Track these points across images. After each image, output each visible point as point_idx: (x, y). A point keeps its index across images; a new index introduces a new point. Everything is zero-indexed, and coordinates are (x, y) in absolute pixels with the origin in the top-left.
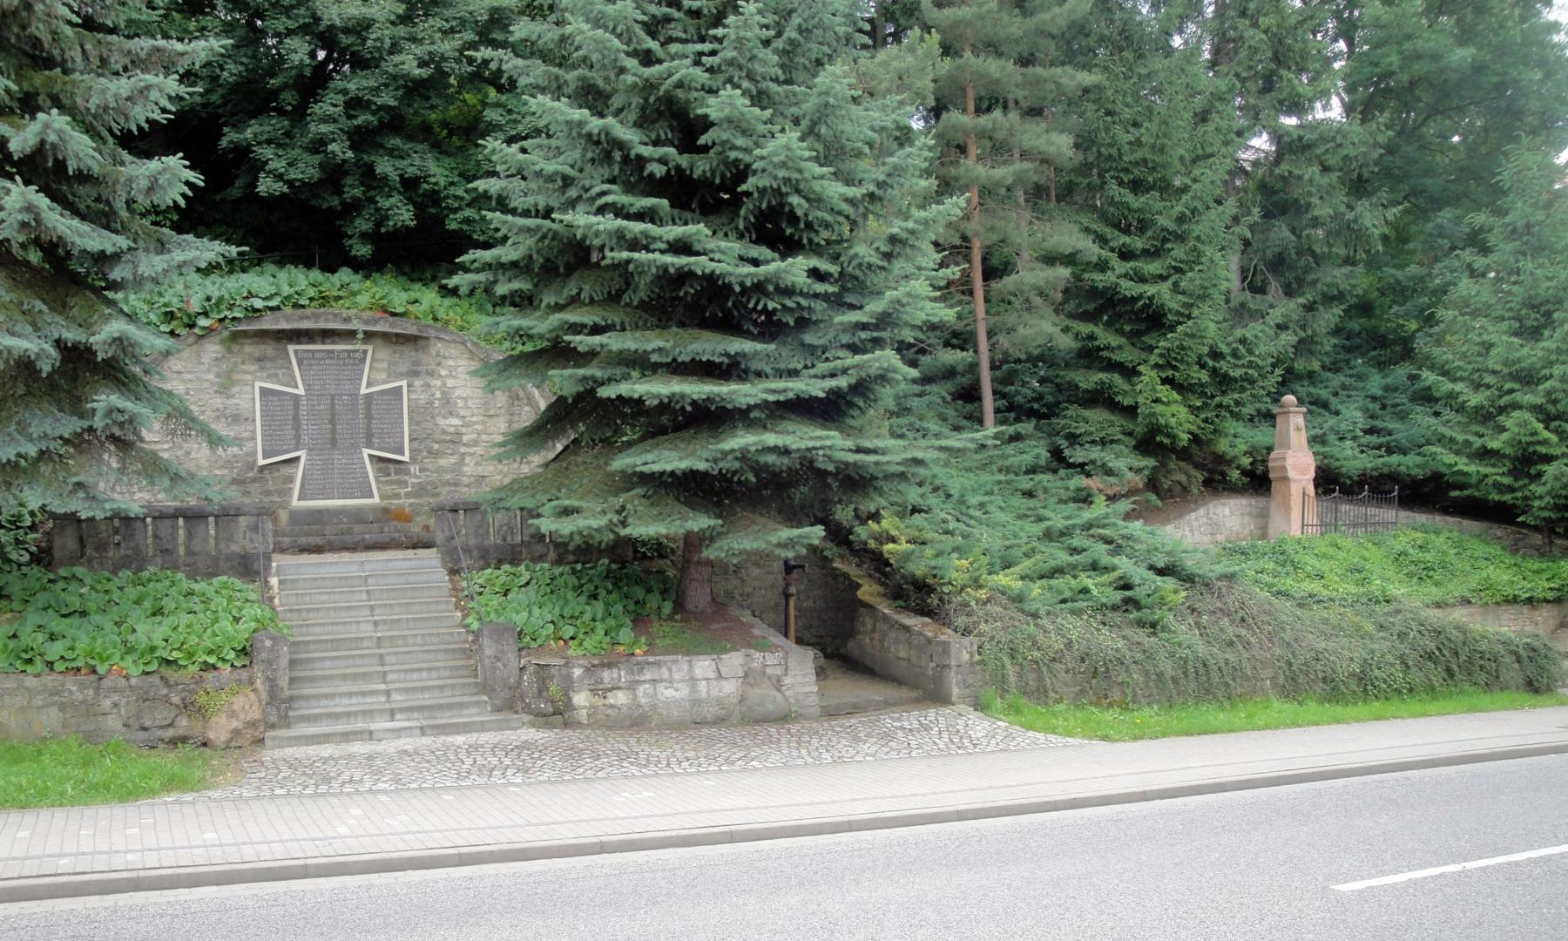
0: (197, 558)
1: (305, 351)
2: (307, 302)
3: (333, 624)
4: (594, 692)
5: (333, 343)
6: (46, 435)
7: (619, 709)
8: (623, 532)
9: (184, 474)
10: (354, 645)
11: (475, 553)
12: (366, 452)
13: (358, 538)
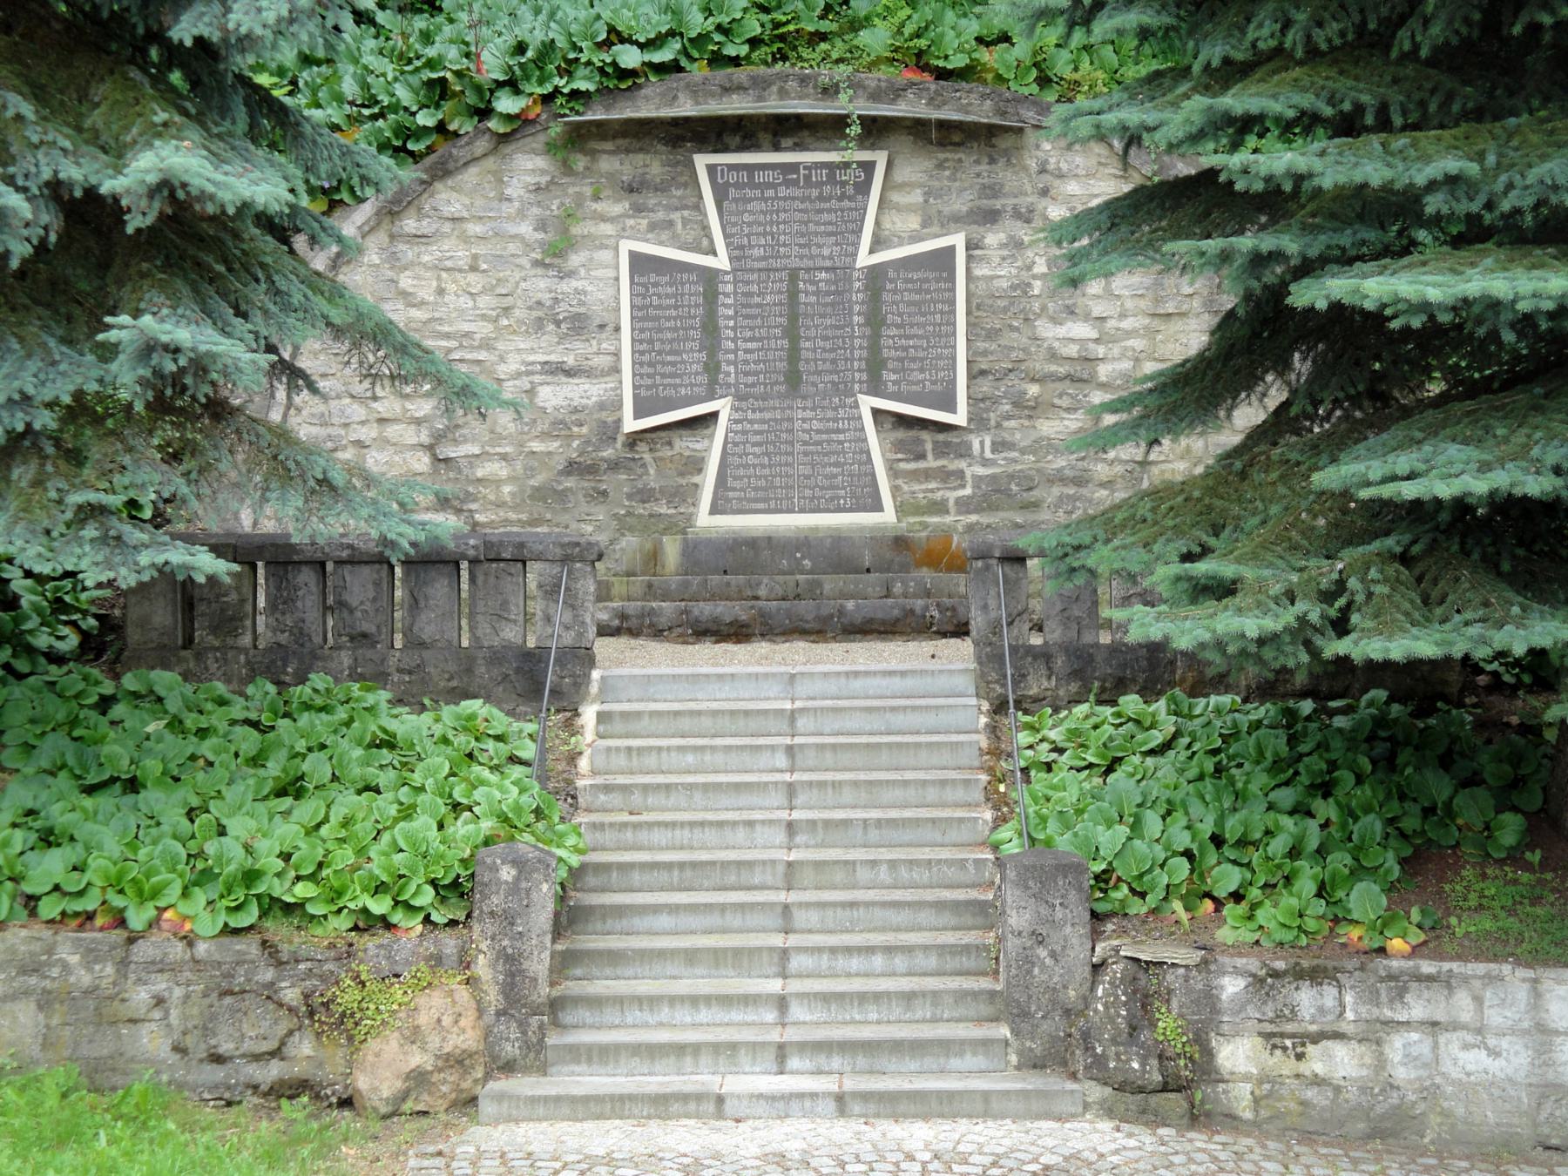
0: (426, 654)
1: (732, 167)
2: (744, 50)
3: (692, 825)
4: (1272, 1039)
5: (799, 147)
6: (26, 398)
7: (1338, 1090)
8: (1335, 647)
9: (338, 478)
10: (732, 879)
11: (1059, 662)
12: (867, 403)
13: (828, 608)
